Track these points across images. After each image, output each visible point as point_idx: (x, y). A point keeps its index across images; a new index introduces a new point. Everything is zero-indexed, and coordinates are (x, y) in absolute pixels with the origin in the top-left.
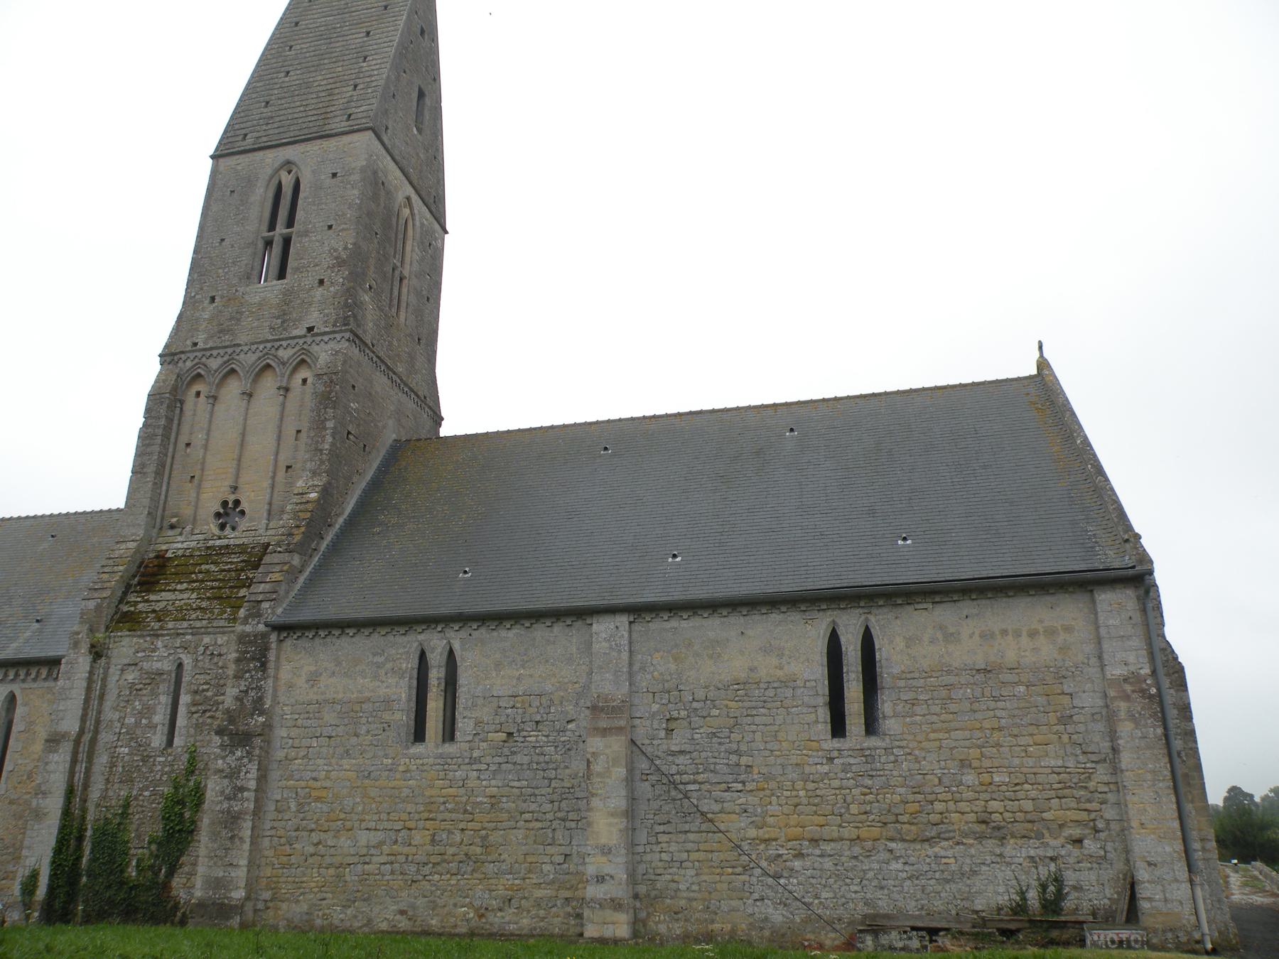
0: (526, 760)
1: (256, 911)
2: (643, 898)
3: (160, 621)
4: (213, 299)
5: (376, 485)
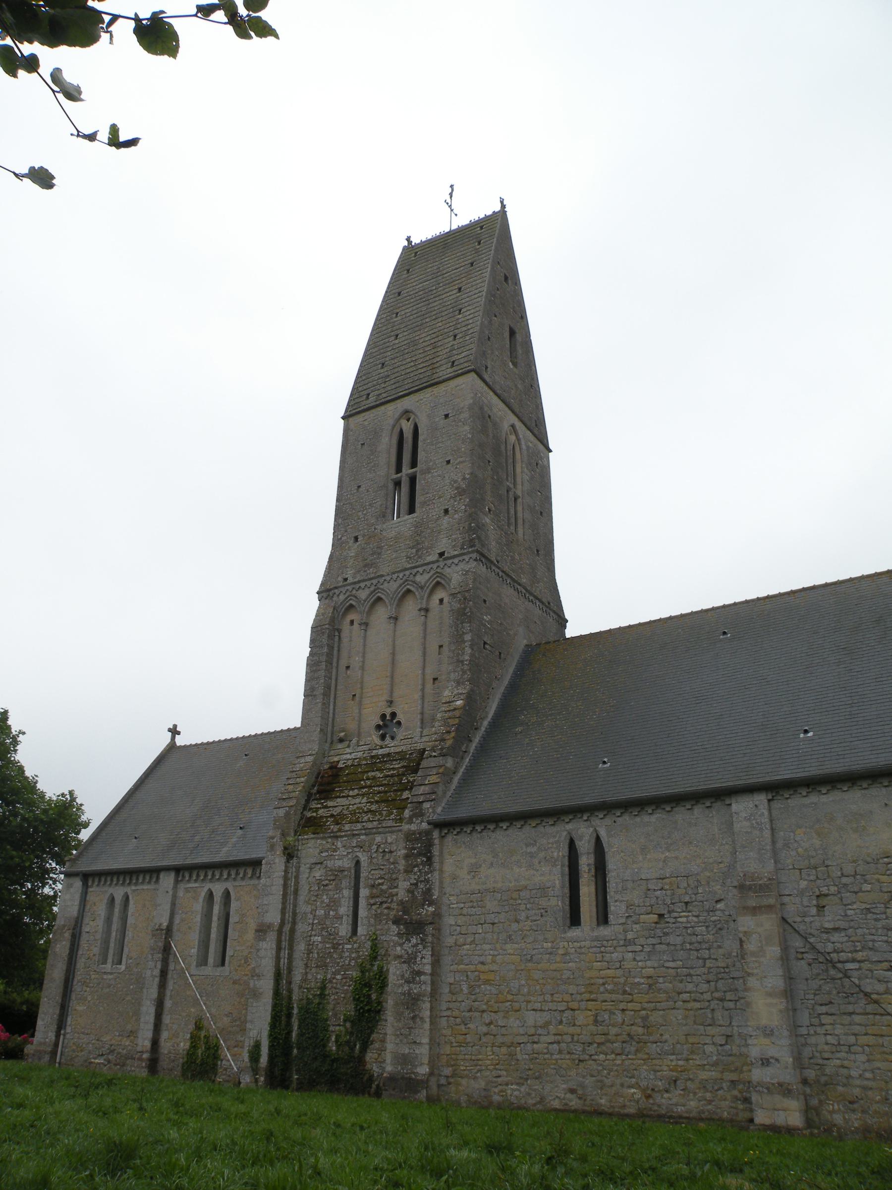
0: (679, 940)
1: (439, 1086)
2: (813, 1085)
3: (338, 824)
4: (356, 539)
5: (513, 688)
